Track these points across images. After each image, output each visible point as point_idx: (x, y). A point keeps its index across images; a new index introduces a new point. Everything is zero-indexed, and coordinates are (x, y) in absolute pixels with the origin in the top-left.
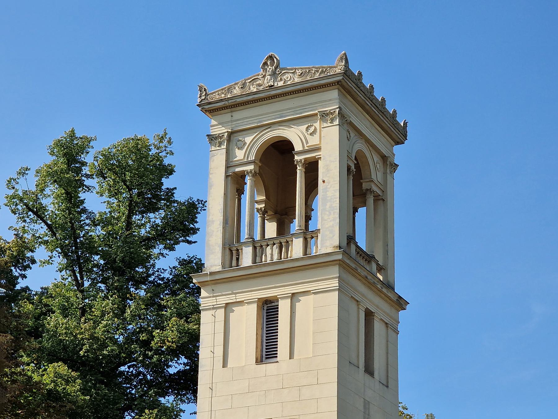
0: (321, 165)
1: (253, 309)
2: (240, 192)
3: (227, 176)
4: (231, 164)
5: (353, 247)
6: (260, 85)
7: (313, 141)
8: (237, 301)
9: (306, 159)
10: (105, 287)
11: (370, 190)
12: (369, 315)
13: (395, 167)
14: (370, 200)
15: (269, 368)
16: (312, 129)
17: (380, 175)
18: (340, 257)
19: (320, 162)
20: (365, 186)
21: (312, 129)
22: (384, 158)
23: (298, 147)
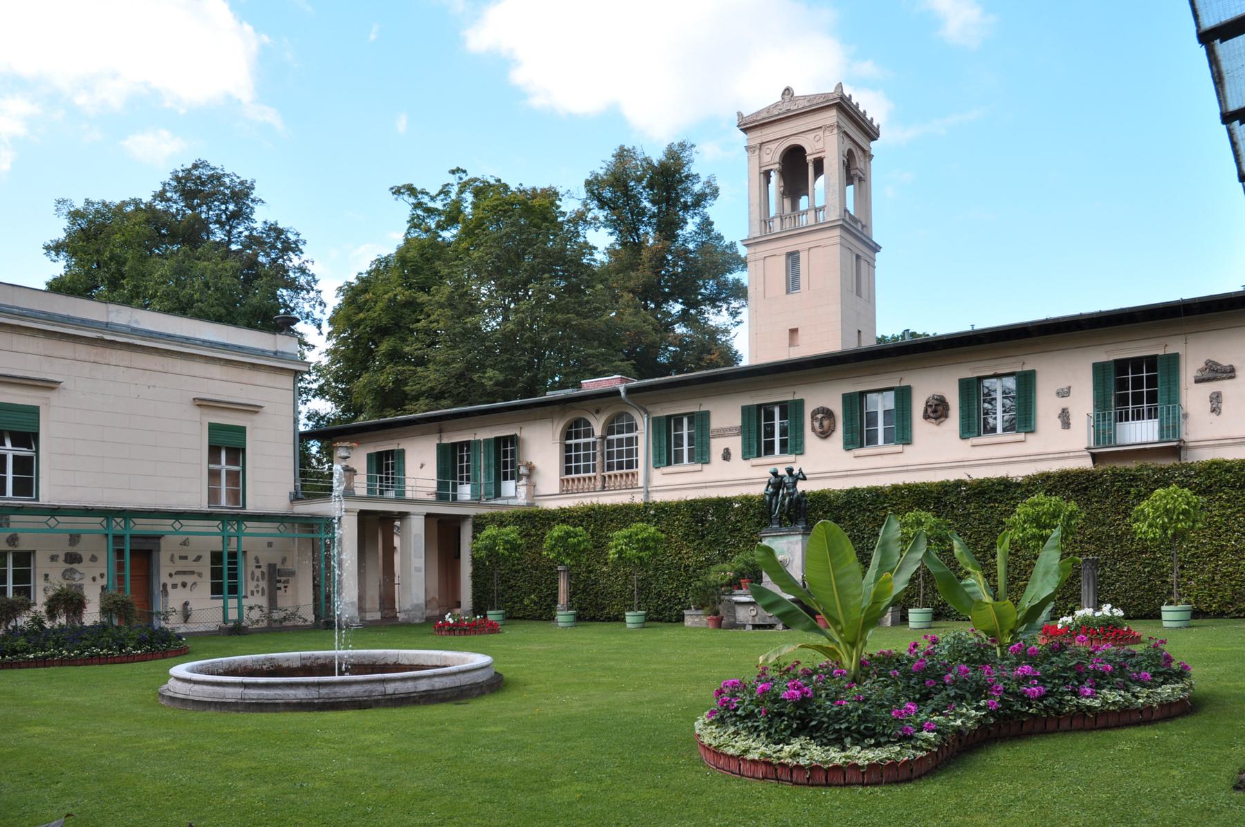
1: (782, 261)
2: (768, 182)
3: (760, 173)
4: (763, 165)
5: (847, 214)
6: (781, 109)
7: (819, 146)
8: (1024, 370)
9: (814, 159)
10: (456, 208)
11: (856, 175)
12: (858, 257)
13: (876, 248)
14: (856, 182)
15: (794, 297)
16: (817, 138)
17: (862, 164)
18: (841, 223)
19: (824, 160)
20: (852, 172)
21: (817, 138)
22: (864, 151)
23: (808, 151)
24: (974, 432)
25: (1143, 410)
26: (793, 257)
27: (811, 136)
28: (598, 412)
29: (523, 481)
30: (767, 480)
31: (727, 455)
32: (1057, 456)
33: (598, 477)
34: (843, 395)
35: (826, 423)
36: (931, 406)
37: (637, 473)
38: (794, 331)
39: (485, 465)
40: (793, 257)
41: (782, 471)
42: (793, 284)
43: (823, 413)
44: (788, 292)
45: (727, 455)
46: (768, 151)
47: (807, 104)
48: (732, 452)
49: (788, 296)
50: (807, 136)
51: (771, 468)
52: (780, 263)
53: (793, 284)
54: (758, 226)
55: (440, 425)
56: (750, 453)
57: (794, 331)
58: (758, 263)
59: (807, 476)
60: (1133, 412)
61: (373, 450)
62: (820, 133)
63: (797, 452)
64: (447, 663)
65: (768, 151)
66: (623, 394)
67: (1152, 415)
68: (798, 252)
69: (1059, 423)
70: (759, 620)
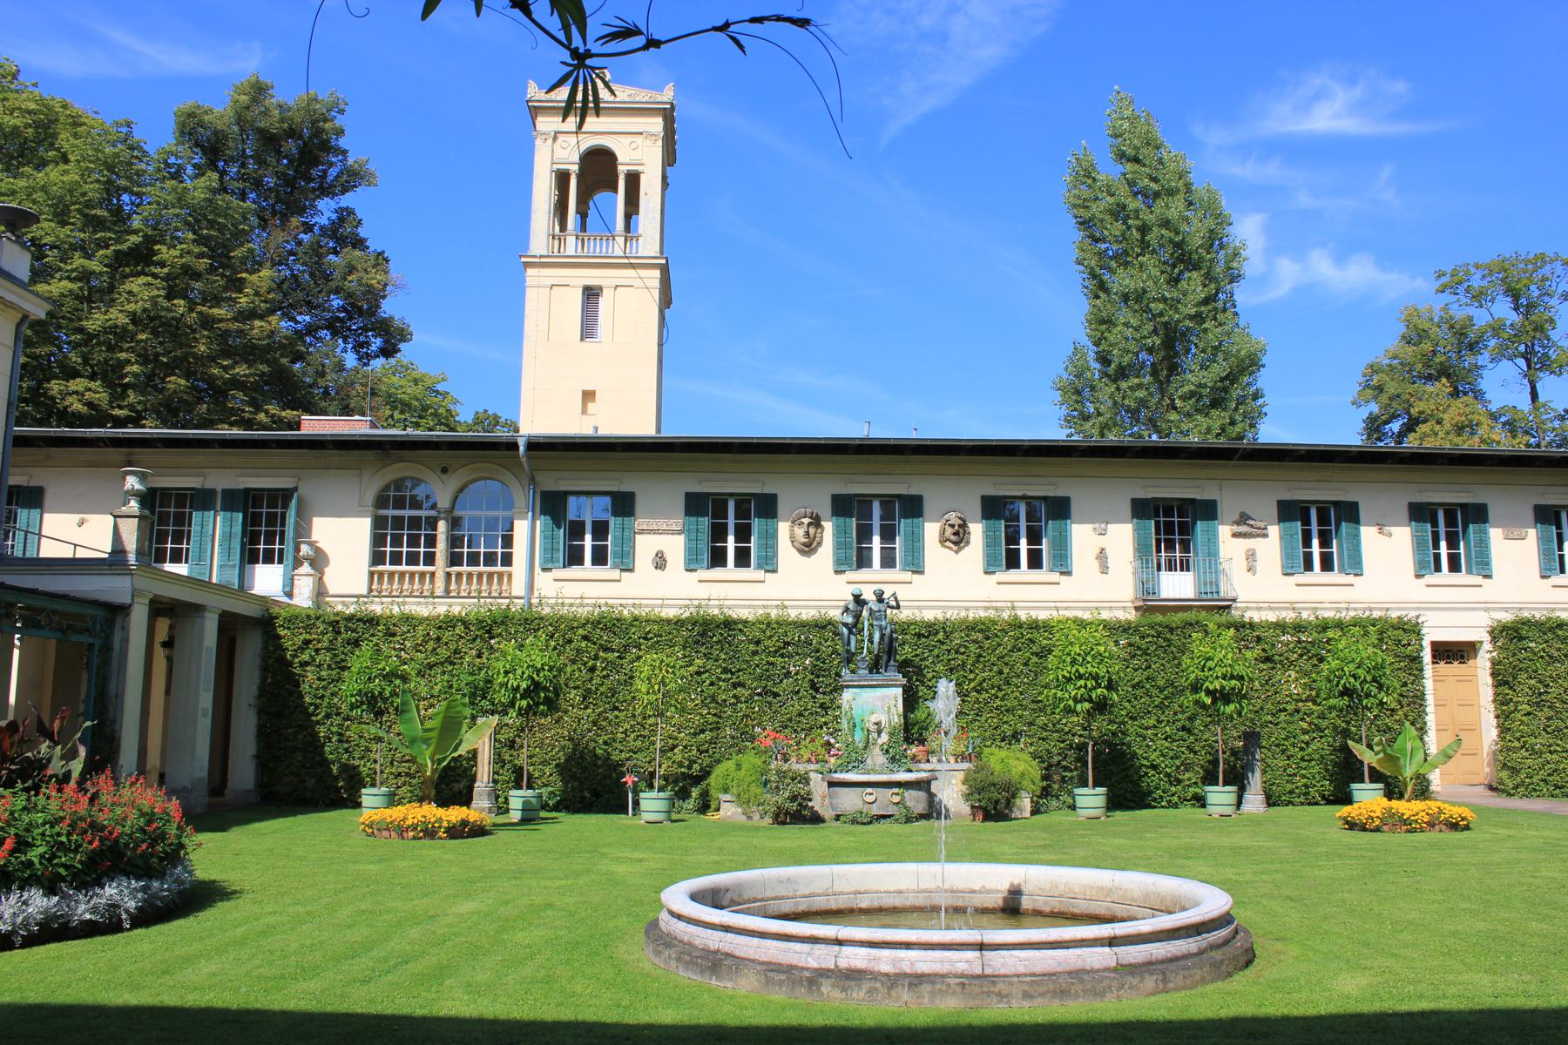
0: (643, 179)
4: (555, 161)
7: (636, 156)
15: (589, 345)
16: (634, 145)
19: (642, 176)
21: (634, 145)
23: (621, 159)
24: (1001, 565)
25: (1175, 560)
26: (591, 294)
27: (626, 140)
28: (445, 470)
29: (306, 568)
30: (842, 603)
31: (660, 562)
32: (1281, 605)
33: (440, 576)
34: (1410, 504)
35: (812, 530)
36: (952, 526)
37: (510, 576)
38: (588, 396)
39: (223, 533)
40: (591, 294)
41: (868, 594)
42: (588, 329)
43: (811, 518)
44: (582, 339)
45: (660, 562)
46: (565, 145)
47: (627, 99)
48: (667, 556)
49: (583, 343)
50: (620, 140)
51: (855, 589)
52: (577, 296)
53: (588, 329)
54: (546, 240)
55: (129, 454)
56: (552, 560)
57: (588, 396)
58: (541, 290)
59: (901, 604)
60: (1181, 561)
61: (1286, 496)
62: (639, 139)
63: (767, 568)
64: (1119, 910)
65: (565, 145)
66: (522, 449)
67: (1185, 566)
68: (601, 288)
69: (1096, 565)
70: (879, 809)
